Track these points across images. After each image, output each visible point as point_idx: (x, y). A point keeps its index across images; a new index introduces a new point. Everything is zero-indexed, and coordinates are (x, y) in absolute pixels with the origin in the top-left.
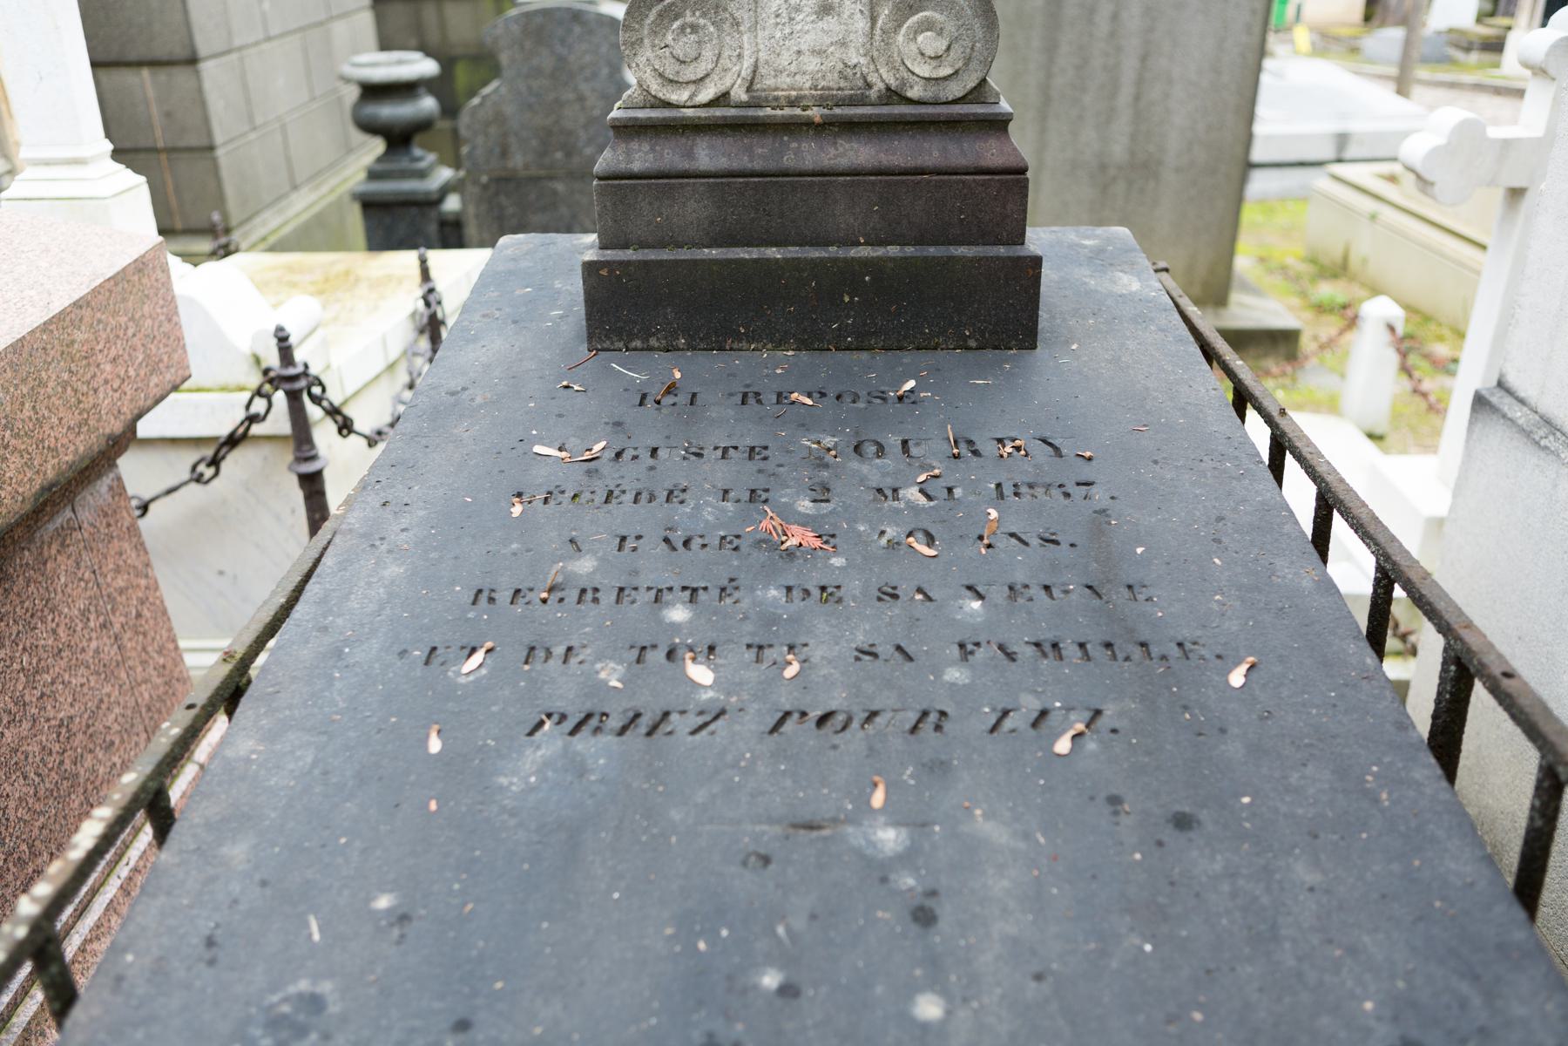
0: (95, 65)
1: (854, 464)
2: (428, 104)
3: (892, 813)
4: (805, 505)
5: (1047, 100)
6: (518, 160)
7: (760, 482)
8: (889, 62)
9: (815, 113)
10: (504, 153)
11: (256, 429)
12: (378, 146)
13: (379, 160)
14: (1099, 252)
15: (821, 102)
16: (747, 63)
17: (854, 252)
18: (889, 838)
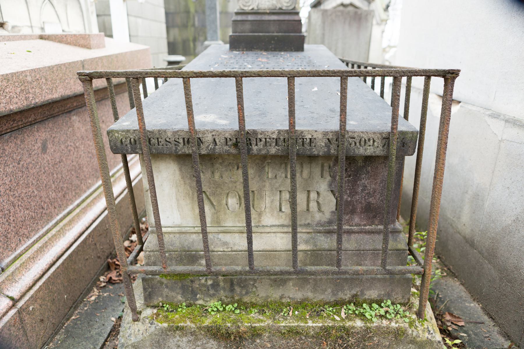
15: (269, 9)
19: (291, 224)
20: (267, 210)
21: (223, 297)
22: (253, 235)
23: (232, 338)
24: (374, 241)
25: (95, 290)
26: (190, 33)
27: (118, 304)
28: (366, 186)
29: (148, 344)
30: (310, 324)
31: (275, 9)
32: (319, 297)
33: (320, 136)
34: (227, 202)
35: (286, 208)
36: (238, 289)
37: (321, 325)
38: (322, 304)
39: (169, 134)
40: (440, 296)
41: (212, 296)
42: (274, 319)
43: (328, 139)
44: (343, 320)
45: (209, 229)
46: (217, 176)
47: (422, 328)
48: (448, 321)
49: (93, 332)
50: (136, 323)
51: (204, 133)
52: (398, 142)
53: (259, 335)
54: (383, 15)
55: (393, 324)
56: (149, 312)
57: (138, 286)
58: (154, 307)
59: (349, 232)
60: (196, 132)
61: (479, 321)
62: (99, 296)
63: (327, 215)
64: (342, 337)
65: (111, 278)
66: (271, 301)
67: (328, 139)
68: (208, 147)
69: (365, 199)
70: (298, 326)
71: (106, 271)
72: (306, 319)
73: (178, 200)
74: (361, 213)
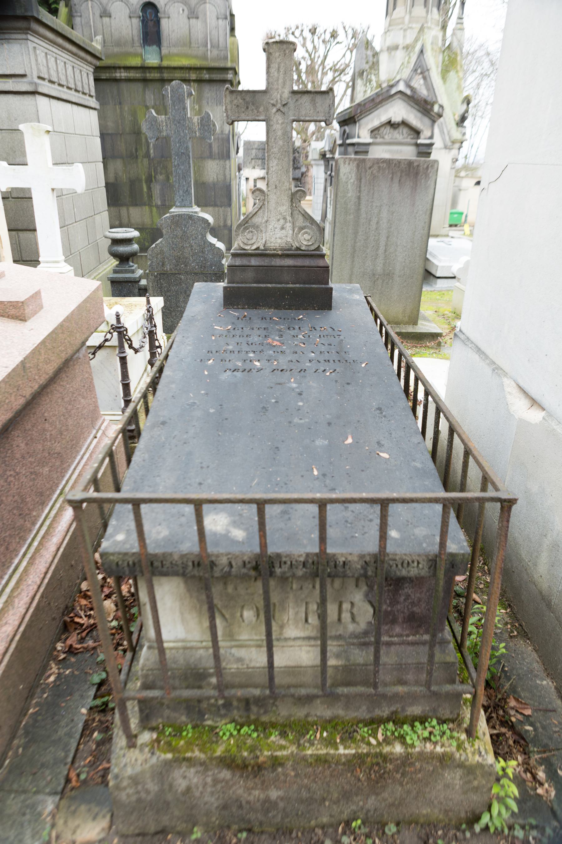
0: (9, 230)
1: (288, 331)
2: (136, 247)
3: (294, 382)
4: (277, 338)
5: (354, 251)
6: (168, 267)
7: (267, 334)
8: (297, 241)
9: (280, 252)
10: (163, 265)
11: (107, 344)
12: (114, 262)
13: (117, 266)
14: (350, 290)
15: (281, 250)
16: (264, 240)
17: (288, 286)
18: (294, 385)
19: (319, 635)
20: (290, 622)
21: (236, 718)
22: (274, 649)
23: (250, 768)
24: (418, 653)
25: (53, 665)
26: (141, 168)
27: (86, 687)
28: (410, 596)
29: (148, 775)
30: (342, 750)
31: (290, 250)
32: (352, 714)
33: (356, 559)
34: (242, 616)
35: (313, 620)
36: (254, 709)
37: (353, 751)
38: (355, 722)
39: (176, 557)
40: (506, 669)
41: (223, 716)
42: (299, 745)
43: (366, 562)
44: (379, 744)
45: (221, 644)
46: (230, 589)
47: (472, 749)
48: (512, 708)
49: (61, 732)
50: (132, 750)
51: (217, 556)
52: (446, 564)
53: (282, 765)
54: (456, 134)
55: (439, 749)
56: (146, 737)
57: (133, 709)
58: (153, 729)
59: (389, 644)
60: (209, 556)
61: (550, 707)
62: (59, 674)
63: (362, 626)
64: (378, 764)
65: (71, 646)
66: (294, 720)
67: (366, 562)
68: (222, 570)
69: (408, 609)
70: (327, 754)
71: (63, 633)
72: (336, 743)
73: (182, 614)
74: (403, 622)
